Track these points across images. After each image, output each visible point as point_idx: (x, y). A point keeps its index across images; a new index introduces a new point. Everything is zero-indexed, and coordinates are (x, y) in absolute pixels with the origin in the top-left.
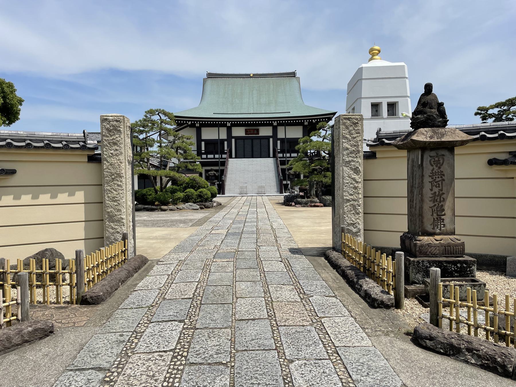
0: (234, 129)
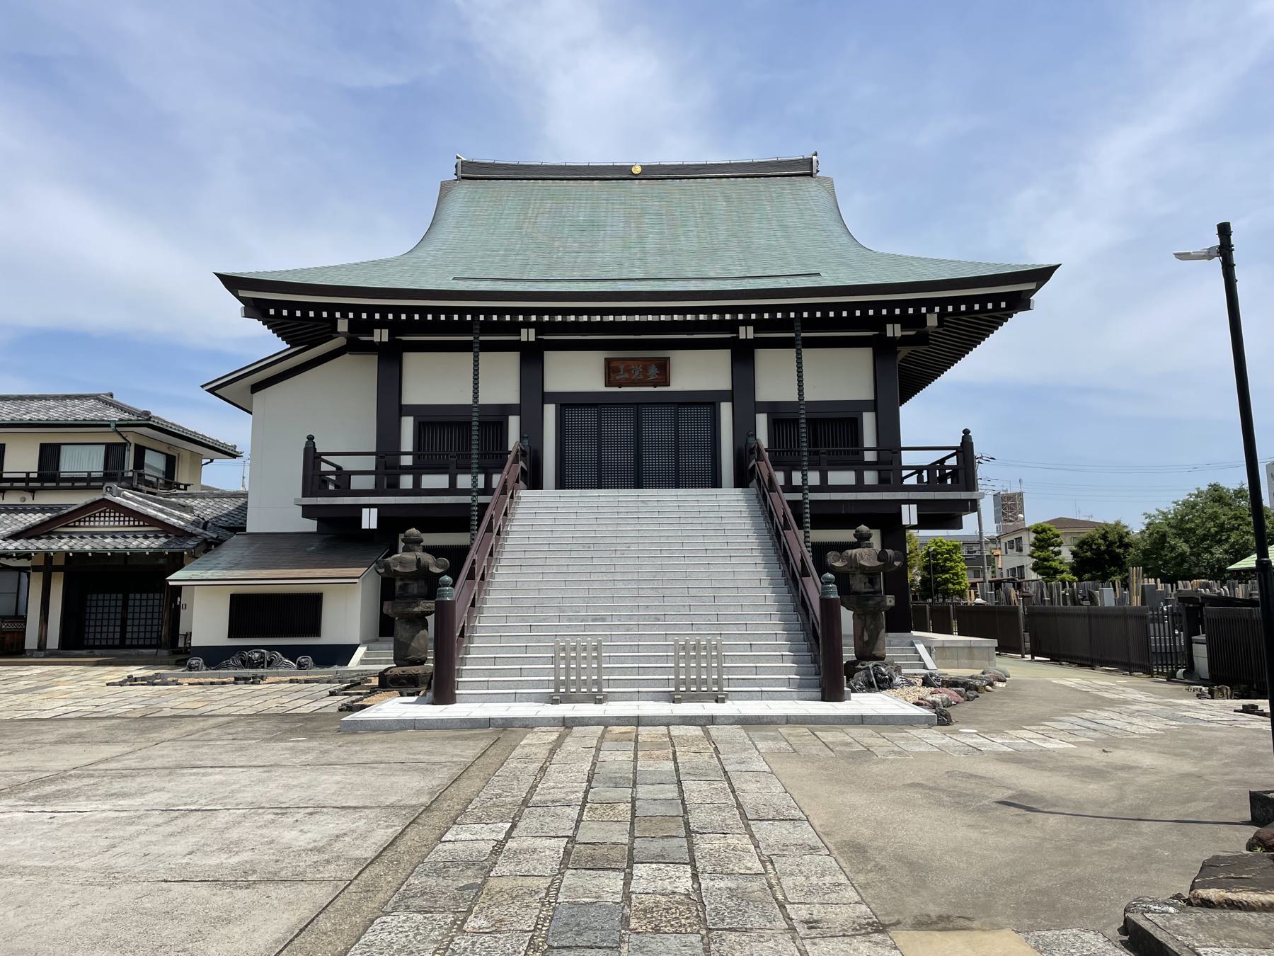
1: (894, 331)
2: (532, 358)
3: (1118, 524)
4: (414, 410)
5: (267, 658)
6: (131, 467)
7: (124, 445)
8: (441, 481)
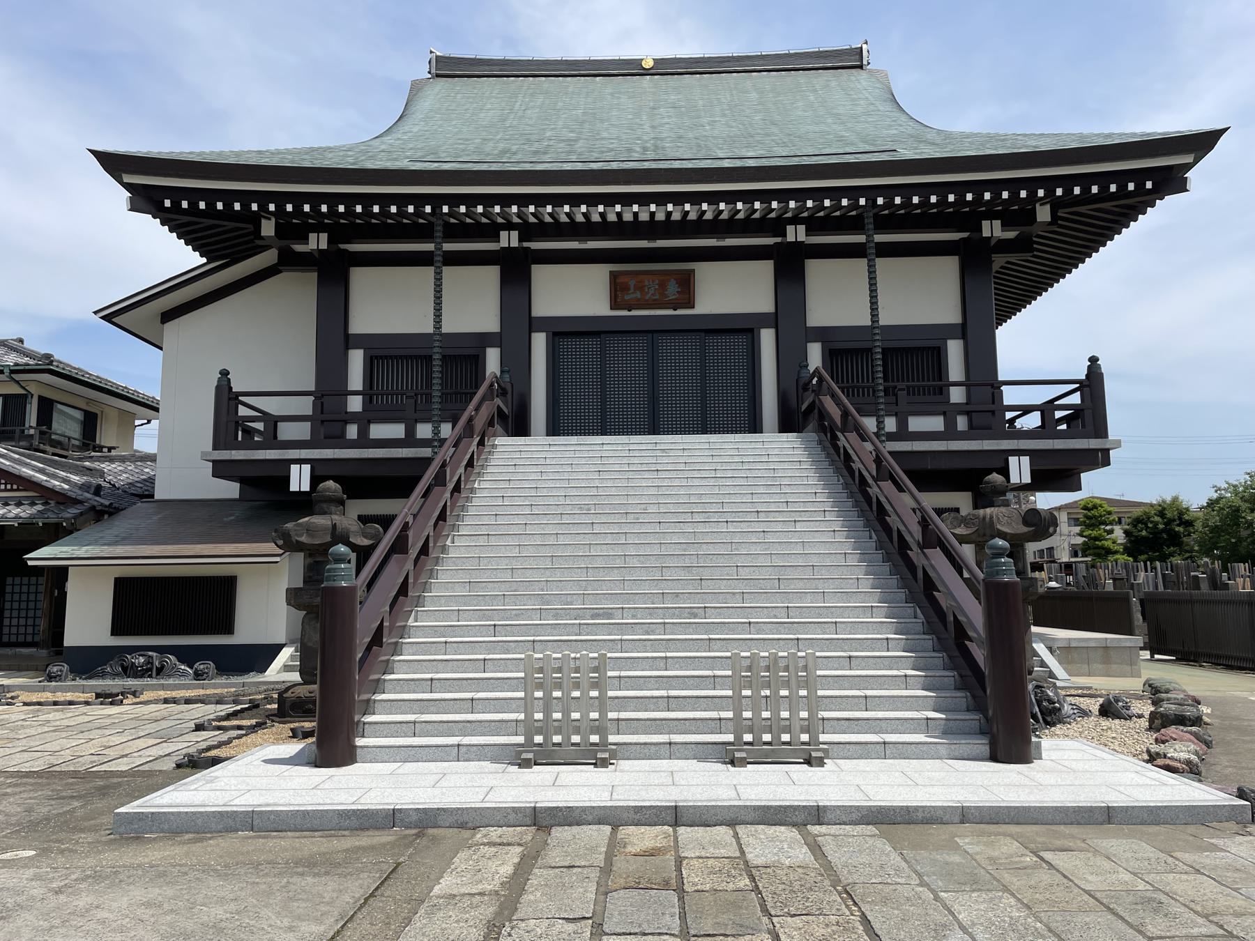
0: (542, 275)
1: (992, 229)
2: (515, 272)
3: (1175, 499)
4: (365, 341)
5: (157, 663)
6: (34, 423)
7: (25, 396)
8: (396, 431)
